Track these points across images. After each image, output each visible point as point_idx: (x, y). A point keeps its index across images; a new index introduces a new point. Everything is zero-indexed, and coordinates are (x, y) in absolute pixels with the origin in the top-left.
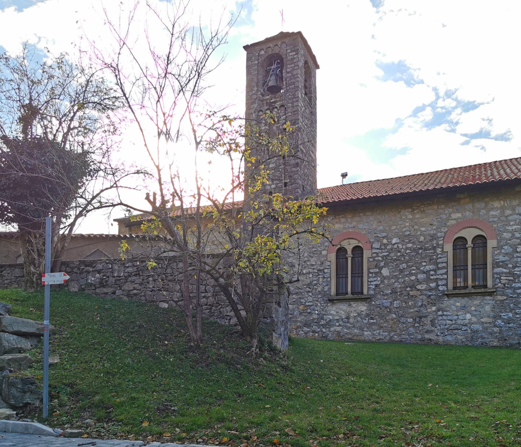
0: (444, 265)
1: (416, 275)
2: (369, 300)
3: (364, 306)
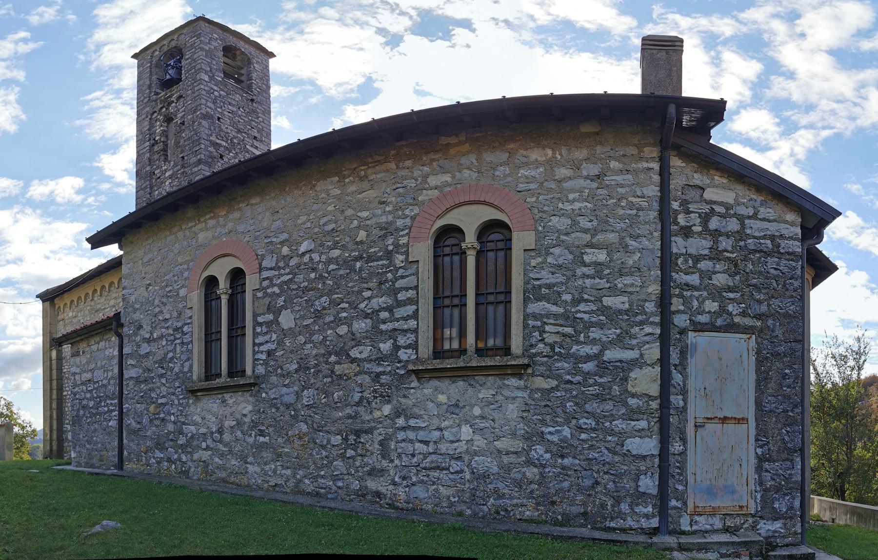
0: (411, 293)
1: (348, 322)
2: (257, 388)
3: (248, 402)
